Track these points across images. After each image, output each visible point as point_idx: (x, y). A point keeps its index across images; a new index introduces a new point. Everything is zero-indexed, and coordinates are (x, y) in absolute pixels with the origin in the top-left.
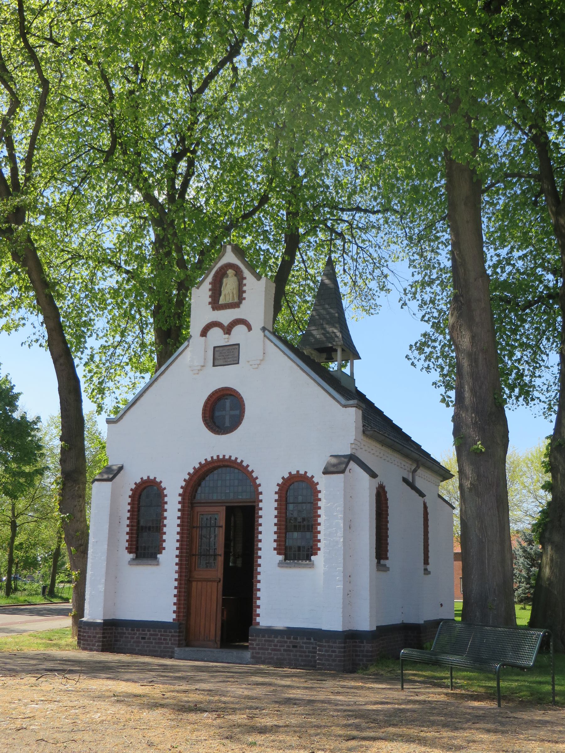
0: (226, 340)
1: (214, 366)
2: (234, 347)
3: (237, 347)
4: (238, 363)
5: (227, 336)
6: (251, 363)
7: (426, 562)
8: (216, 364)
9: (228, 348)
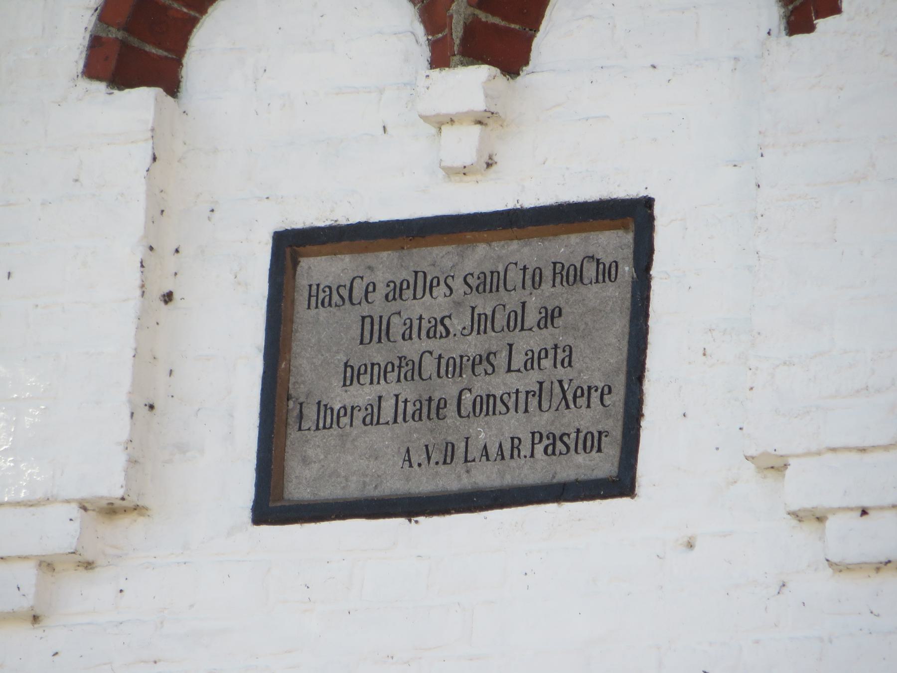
0: (463, 144)
1: (273, 505)
2: (569, 247)
3: (613, 244)
4: (621, 485)
5: (472, 82)
6: (803, 486)
7: (834, 450)
8: (300, 486)
9: (481, 256)
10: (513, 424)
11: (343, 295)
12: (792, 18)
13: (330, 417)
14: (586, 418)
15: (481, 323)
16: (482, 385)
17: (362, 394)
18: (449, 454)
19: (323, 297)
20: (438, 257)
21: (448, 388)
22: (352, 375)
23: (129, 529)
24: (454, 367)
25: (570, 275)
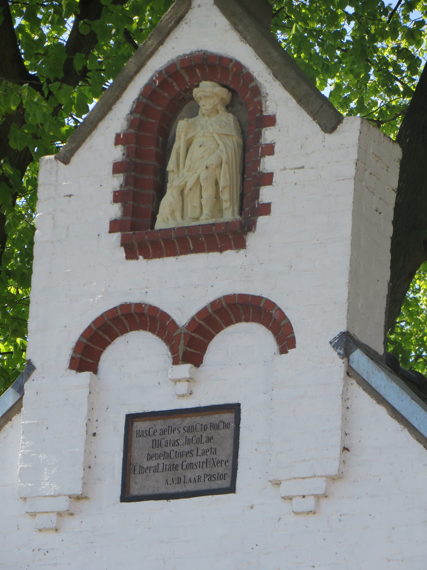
0: (183, 388)
4: (232, 489)
5: (185, 369)
6: (286, 489)
8: (134, 491)
9: (188, 421)
10: (198, 472)
13: (143, 470)
14: (220, 470)
15: (188, 442)
16: (189, 460)
17: (153, 463)
18: (179, 481)
19: (141, 434)
20: (176, 422)
21: (179, 461)
22: (150, 457)
23: (84, 504)
24: (181, 455)
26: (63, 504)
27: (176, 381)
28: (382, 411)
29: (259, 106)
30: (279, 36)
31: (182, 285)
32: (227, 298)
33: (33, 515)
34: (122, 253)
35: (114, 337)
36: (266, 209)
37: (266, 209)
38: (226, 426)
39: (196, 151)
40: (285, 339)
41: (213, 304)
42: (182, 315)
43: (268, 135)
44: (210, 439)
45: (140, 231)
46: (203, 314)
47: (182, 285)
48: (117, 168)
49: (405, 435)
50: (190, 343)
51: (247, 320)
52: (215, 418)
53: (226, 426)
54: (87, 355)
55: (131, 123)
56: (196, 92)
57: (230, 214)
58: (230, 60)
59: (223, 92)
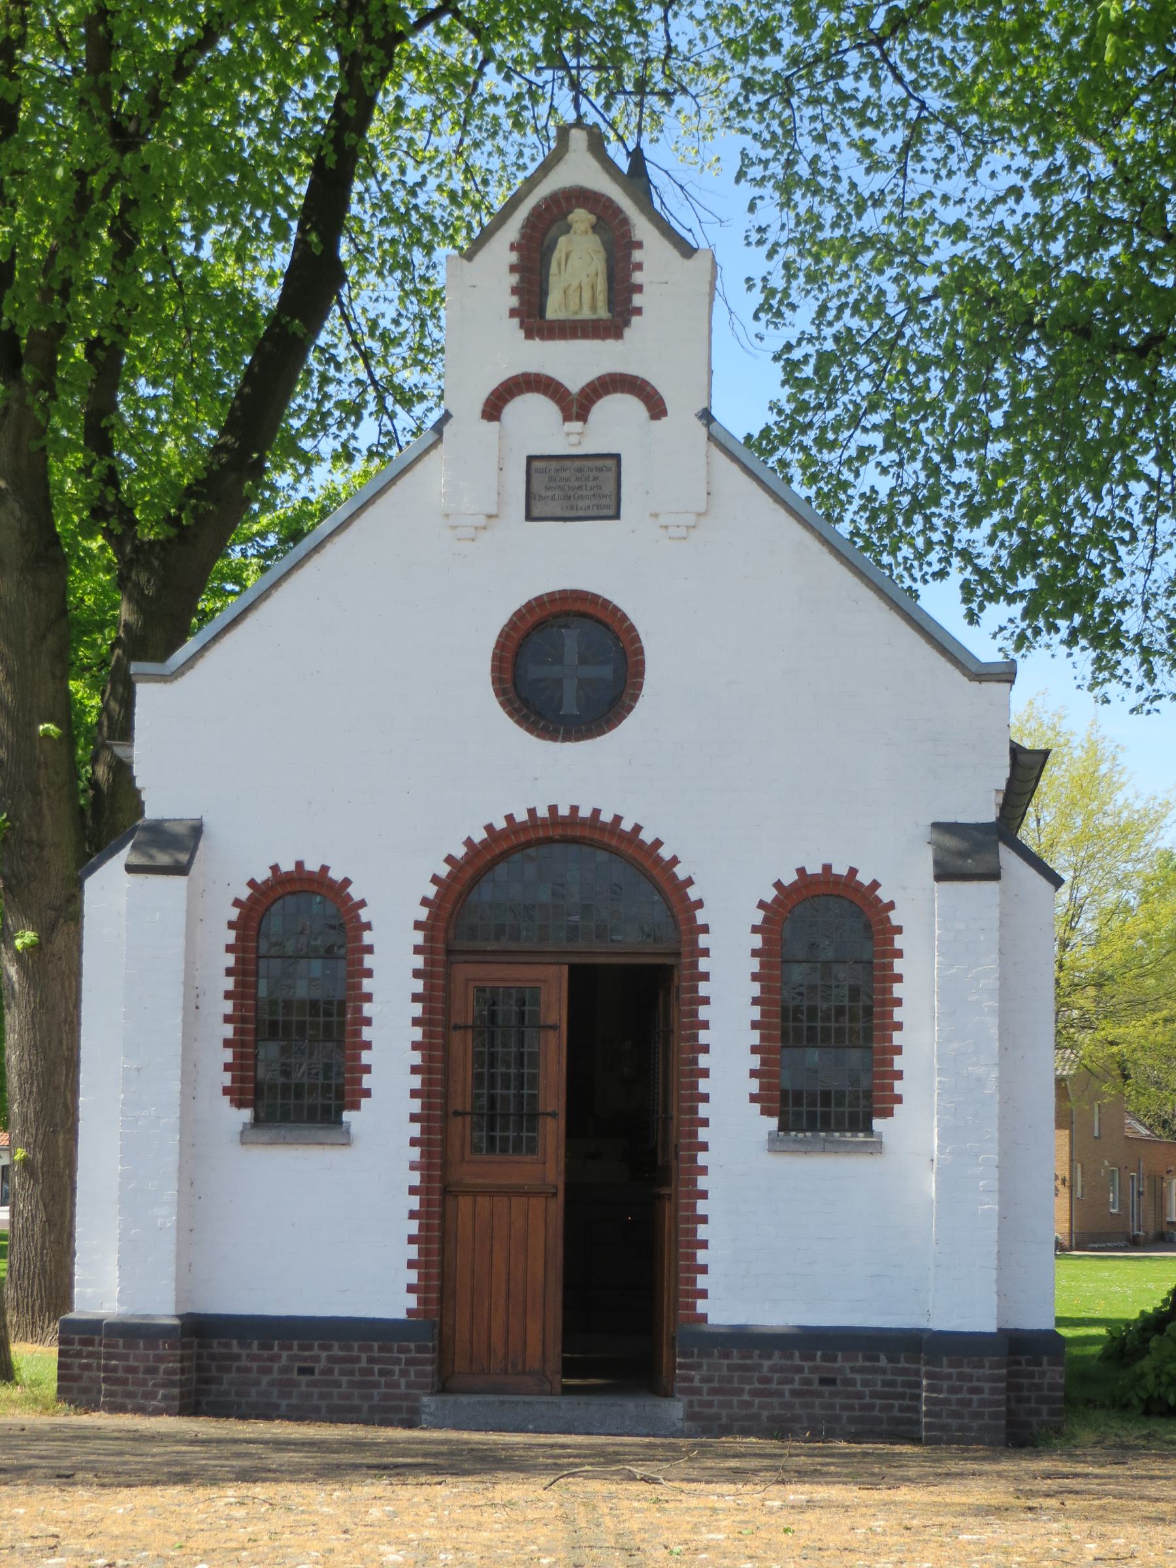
0: (574, 439)
1: (529, 517)
4: (617, 516)
5: (576, 426)
6: (663, 520)
8: (536, 512)
9: (577, 464)
10: (587, 502)
11: (545, 471)
12: (247, 390)
13: (541, 498)
14: (606, 502)
15: (578, 479)
16: (579, 493)
17: (550, 493)
18: (572, 508)
19: (539, 471)
20: (567, 463)
21: (571, 493)
22: (547, 489)
23: (495, 521)
24: (573, 489)
25: (600, 470)
26: (482, 521)
27: (568, 434)
28: (734, 468)
29: (627, 233)
30: (303, 190)
31: (575, 362)
32: (610, 375)
33: (454, 527)
34: (522, 334)
35: (615, 391)
36: (638, 311)
37: (638, 311)
38: (609, 470)
39: (574, 260)
40: (656, 408)
41: (599, 378)
42: (575, 384)
43: (637, 256)
44: (595, 479)
45: (533, 317)
46: (591, 385)
47: (575, 362)
48: (513, 269)
49: (753, 486)
50: (576, 406)
51: (622, 392)
52: (599, 463)
53: (609, 470)
54: (493, 409)
55: (523, 236)
56: (570, 217)
57: (603, 313)
58: (603, 196)
59: (592, 218)
